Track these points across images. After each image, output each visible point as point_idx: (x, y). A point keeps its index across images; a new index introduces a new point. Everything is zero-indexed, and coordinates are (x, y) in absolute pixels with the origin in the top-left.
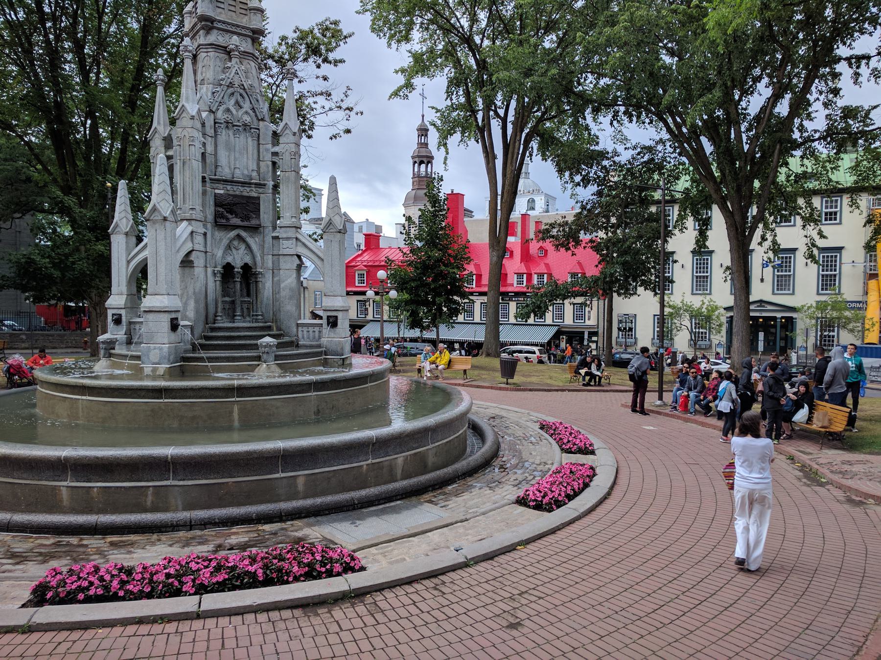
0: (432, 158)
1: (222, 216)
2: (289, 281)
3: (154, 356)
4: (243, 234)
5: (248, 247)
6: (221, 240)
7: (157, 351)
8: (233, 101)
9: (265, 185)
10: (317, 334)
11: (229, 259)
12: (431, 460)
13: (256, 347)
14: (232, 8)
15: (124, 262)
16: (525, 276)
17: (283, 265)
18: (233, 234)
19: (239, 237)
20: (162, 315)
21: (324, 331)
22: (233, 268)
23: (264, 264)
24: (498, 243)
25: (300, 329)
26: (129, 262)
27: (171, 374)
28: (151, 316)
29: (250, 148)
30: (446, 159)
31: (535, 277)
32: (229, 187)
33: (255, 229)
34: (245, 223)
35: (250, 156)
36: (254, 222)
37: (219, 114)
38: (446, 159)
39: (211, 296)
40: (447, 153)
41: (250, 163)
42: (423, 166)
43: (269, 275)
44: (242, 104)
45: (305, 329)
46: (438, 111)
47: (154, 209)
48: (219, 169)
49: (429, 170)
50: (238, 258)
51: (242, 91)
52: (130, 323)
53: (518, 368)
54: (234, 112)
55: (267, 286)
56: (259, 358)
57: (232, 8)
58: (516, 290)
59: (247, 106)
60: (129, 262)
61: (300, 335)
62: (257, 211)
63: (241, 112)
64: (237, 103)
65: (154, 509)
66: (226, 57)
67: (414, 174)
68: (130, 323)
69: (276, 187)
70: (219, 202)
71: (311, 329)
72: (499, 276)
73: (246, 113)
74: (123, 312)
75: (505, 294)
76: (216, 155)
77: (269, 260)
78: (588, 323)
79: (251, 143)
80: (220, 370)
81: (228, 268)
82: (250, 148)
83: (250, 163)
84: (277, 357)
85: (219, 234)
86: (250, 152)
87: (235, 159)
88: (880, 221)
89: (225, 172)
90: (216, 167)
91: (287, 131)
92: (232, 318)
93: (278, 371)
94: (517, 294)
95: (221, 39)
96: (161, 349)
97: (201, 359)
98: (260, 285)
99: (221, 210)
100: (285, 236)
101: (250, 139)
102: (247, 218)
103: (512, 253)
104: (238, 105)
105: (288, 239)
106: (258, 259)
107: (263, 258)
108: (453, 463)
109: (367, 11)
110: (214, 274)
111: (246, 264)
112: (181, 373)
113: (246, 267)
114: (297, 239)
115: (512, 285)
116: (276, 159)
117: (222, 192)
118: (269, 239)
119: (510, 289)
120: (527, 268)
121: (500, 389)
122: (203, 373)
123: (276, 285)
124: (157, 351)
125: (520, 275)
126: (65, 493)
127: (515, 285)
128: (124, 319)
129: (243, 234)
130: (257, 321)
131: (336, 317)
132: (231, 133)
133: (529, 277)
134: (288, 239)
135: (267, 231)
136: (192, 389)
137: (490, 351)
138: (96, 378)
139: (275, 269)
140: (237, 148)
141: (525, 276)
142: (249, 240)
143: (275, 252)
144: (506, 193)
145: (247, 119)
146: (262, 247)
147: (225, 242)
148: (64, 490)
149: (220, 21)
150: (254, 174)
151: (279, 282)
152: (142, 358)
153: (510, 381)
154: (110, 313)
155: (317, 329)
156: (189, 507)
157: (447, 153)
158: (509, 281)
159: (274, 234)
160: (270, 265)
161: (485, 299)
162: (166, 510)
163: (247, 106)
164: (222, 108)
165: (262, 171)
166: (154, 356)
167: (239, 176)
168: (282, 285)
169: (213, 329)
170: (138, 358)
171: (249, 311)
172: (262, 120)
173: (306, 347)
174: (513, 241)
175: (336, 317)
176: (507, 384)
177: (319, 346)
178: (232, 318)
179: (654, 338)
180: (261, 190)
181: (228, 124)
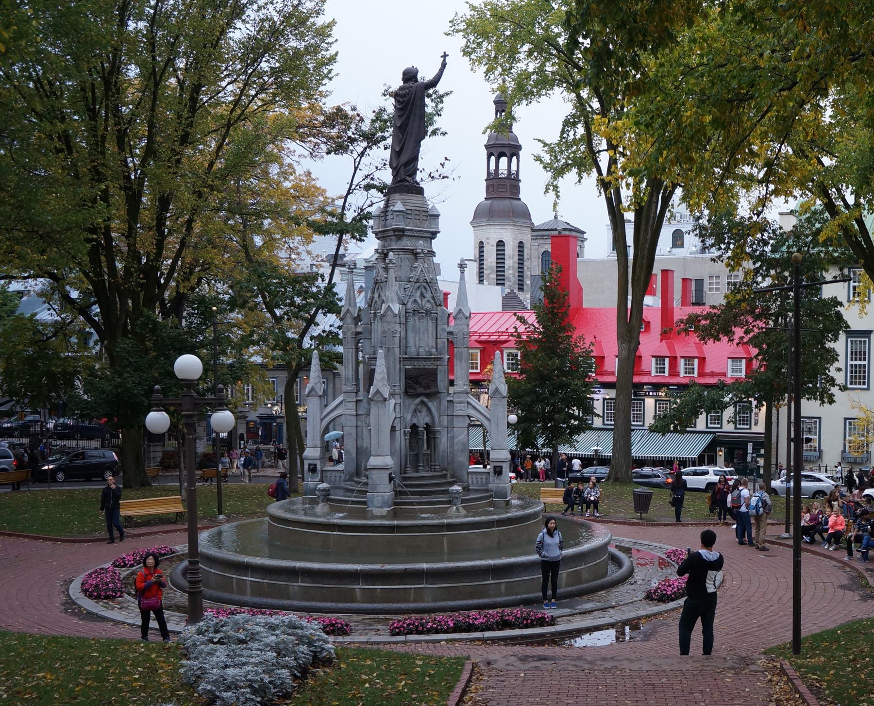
0: (519, 147)
1: (411, 387)
2: (462, 437)
3: (378, 501)
4: (426, 400)
5: (429, 410)
6: (409, 406)
7: (380, 498)
8: (418, 294)
9: (441, 358)
10: (484, 480)
11: (415, 421)
12: (585, 576)
13: (446, 492)
14: (417, 217)
15: (319, 420)
16: (667, 360)
17: (456, 424)
18: (418, 400)
19: (422, 402)
20: (383, 471)
21: (491, 478)
22: (418, 427)
23: (441, 423)
24: (631, 325)
25: (470, 476)
26: (322, 420)
27: (395, 514)
28: (374, 472)
29: (430, 329)
30: (555, 204)
31: (682, 362)
32: (415, 363)
33: (432, 396)
34: (427, 392)
35: (430, 336)
36: (433, 390)
37: (409, 306)
38: (555, 204)
39: (403, 452)
40: (558, 196)
41: (430, 341)
42: (504, 161)
43: (444, 433)
44: (425, 295)
45: (474, 477)
46: (545, 145)
47: (378, 392)
48: (409, 349)
49: (514, 167)
50: (422, 420)
51: (425, 284)
52: (322, 471)
53: (652, 503)
54: (420, 302)
55: (443, 441)
56: (449, 502)
57: (417, 217)
58: (654, 381)
59: (428, 296)
60: (322, 420)
61: (470, 482)
62: (435, 380)
63: (425, 300)
64: (422, 294)
65: (415, 601)
66: (413, 257)
67: (489, 173)
68: (322, 471)
69: (451, 361)
70: (408, 377)
71: (479, 476)
72: (631, 360)
73: (428, 301)
74: (318, 463)
75: (639, 386)
76: (406, 338)
77: (445, 420)
78: (754, 429)
79: (431, 325)
80: (422, 511)
81: (414, 427)
82: (430, 329)
83: (430, 341)
84: (463, 501)
85: (408, 401)
86: (430, 332)
87: (420, 340)
88: (278, 705)
89: (412, 351)
90: (407, 347)
91: (461, 315)
92: (416, 469)
93: (463, 512)
94: (657, 387)
95: (409, 243)
96: (383, 497)
97: (411, 504)
98: (438, 441)
99: (409, 381)
100: (458, 400)
101: (430, 322)
102: (427, 387)
103: (648, 324)
104: (422, 296)
105: (460, 402)
106: (437, 418)
107: (439, 418)
108: (600, 578)
109: (458, 31)
110: (405, 434)
111: (427, 424)
112: (395, 514)
113: (428, 427)
114: (468, 403)
115: (649, 373)
116: (451, 338)
117: (410, 367)
118: (444, 403)
119: (645, 379)
120: (671, 347)
121: (634, 524)
122: (413, 515)
123: (452, 439)
124: (380, 498)
125: (660, 359)
126: (358, 592)
127: (653, 373)
128: (319, 468)
129: (426, 400)
130: (435, 471)
131: (501, 467)
132: (416, 318)
133: (674, 360)
134: (460, 402)
135: (442, 395)
136: (416, 526)
137: (619, 475)
138: (316, 516)
139: (450, 427)
140: (421, 331)
141: (667, 360)
142: (430, 404)
143: (450, 413)
144: (638, 269)
145: (428, 306)
146: (439, 409)
147: (413, 407)
148: (357, 590)
149: (409, 230)
150: (434, 350)
151: (453, 437)
152: (368, 503)
153: (644, 515)
154: (306, 463)
155: (484, 476)
156: (435, 601)
157: (558, 196)
158: (644, 367)
159: (449, 399)
160: (445, 423)
161: (612, 394)
162: (423, 602)
163: (428, 296)
164: (411, 300)
165: (439, 347)
166: (378, 501)
167: (423, 353)
168: (456, 441)
169: (405, 479)
170: (364, 503)
171: (430, 463)
172: (440, 305)
173: (477, 491)
174: (652, 302)
175: (501, 467)
176: (641, 519)
177: (487, 491)
178: (416, 469)
179: (844, 451)
180: (438, 363)
181: (415, 312)
